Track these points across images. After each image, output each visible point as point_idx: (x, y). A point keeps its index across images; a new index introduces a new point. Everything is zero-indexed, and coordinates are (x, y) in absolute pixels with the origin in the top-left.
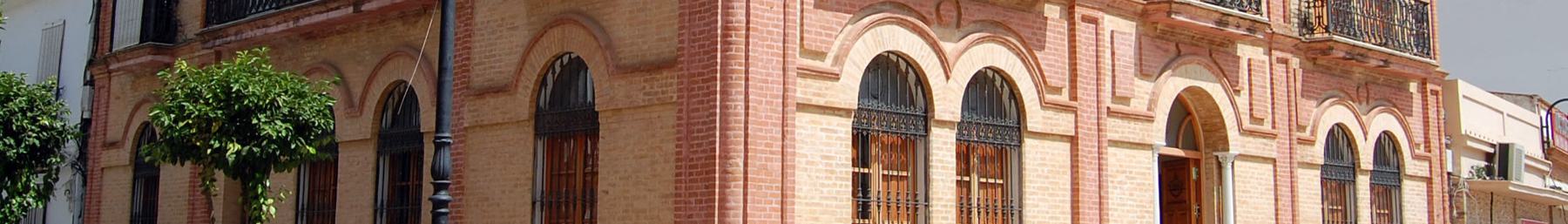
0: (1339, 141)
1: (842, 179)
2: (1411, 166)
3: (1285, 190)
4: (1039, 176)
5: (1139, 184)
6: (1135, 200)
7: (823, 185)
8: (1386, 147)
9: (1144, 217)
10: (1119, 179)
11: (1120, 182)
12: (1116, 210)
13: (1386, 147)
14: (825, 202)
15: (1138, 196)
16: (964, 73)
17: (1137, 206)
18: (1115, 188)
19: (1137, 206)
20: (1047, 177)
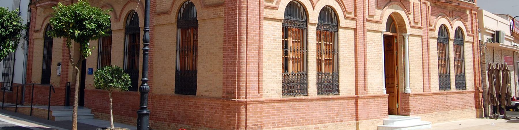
0: (443, 30)
1: (279, 42)
2: (467, 38)
3: (425, 46)
4: (344, 42)
5: (377, 44)
6: (376, 50)
7: (272, 45)
8: (459, 32)
9: (379, 55)
10: (370, 42)
11: (371, 44)
12: (369, 53)
13: (459, 32)
14: (273, 50)
15: (377, 48)
16: (319, 8)
17: (376, 51)
18: (369, 45)
19: (376, 51)
20: (347, 42)
